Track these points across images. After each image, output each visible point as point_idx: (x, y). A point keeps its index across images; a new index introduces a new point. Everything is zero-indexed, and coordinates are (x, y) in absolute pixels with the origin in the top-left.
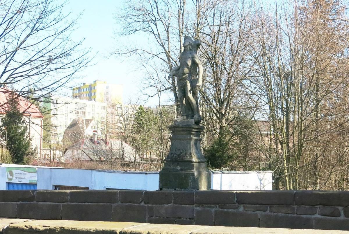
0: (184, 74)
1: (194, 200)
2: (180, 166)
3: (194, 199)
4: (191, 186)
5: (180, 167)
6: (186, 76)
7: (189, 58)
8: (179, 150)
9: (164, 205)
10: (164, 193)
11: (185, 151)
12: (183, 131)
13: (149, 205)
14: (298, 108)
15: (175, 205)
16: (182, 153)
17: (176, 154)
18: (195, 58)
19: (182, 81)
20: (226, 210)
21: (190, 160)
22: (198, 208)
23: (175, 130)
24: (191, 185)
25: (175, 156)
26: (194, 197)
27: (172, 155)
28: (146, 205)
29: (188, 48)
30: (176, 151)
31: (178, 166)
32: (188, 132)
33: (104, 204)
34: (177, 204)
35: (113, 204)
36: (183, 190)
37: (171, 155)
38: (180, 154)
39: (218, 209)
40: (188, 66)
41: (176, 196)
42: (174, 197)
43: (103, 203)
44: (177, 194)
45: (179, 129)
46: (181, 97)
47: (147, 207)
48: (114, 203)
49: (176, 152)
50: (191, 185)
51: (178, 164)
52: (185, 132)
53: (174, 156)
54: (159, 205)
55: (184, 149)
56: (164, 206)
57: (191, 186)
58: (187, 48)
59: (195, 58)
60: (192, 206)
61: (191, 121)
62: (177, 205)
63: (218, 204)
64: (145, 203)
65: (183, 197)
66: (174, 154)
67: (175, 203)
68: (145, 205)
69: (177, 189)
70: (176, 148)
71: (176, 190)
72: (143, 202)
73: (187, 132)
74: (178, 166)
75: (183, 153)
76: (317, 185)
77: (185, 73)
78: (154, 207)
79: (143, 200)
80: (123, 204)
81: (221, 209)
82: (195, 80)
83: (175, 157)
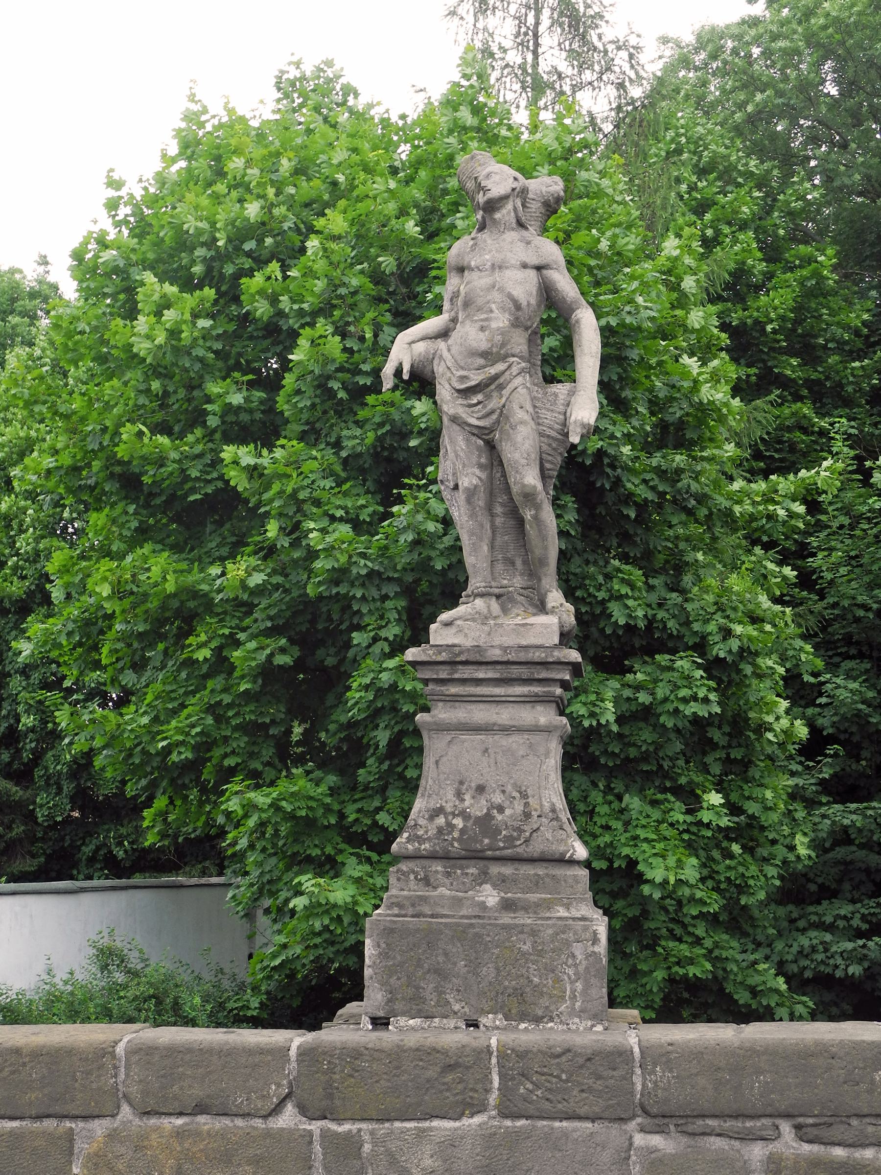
1: (632, 1093)
2: (495, 886)
3: (639, 1087)
4: (578, 1004)
5: (495, 893)
8: (481, 789)
9: (436, 1123)
10: (398, 1054)
11: (517, 795)
13: (333, 1126)
15: (508, 1123)
16: (501, 809)
17: (464, 814)
20: (839, 1152)
21: (562, 848)
22: (656, 1140)
24: (574, 998)
25: (459, 822)
26: (638, 1071)
27: (441, 821)
28: (315, 1127)
30: (459, 795)
31: (487, 887)
33: (15, 1124)
34: (519, 1117)
35: (81, 1124)
36: (523, 1026)
37: (431, 818)
38: (488, 816)
39: (789, 1143)
41: (517, 1063)
42: (501, 1076)
43: (12, 1118)
44: (522, 1054)
47: (316, 1137)
48: (85, 1118)
49: (463, 800)
50: (574, 998)
51: (484, 878)
53: (451, 826)
54: (397, 1124)
55: (509, 788)
56: (431, 1129)
57: (578, 1004)
60: (615, 1129)
62: (521, 1123)
63: (788, 1116)
64: (303, 1110)
65: (564, 1077)
66: (454, 815)
67: (504, 1114)
68: (309, 1128)
69: (484, 1020)
70: (461, 783)
71: (476, 1026)
72: (290, 1109)
74: (481, 884)
75: (508, 812)
76: (757, 792)
78: (366, 1137)
79: (288, 1096)
80: (153, 1121)
81: (806, 1148)
83: (463, 831)
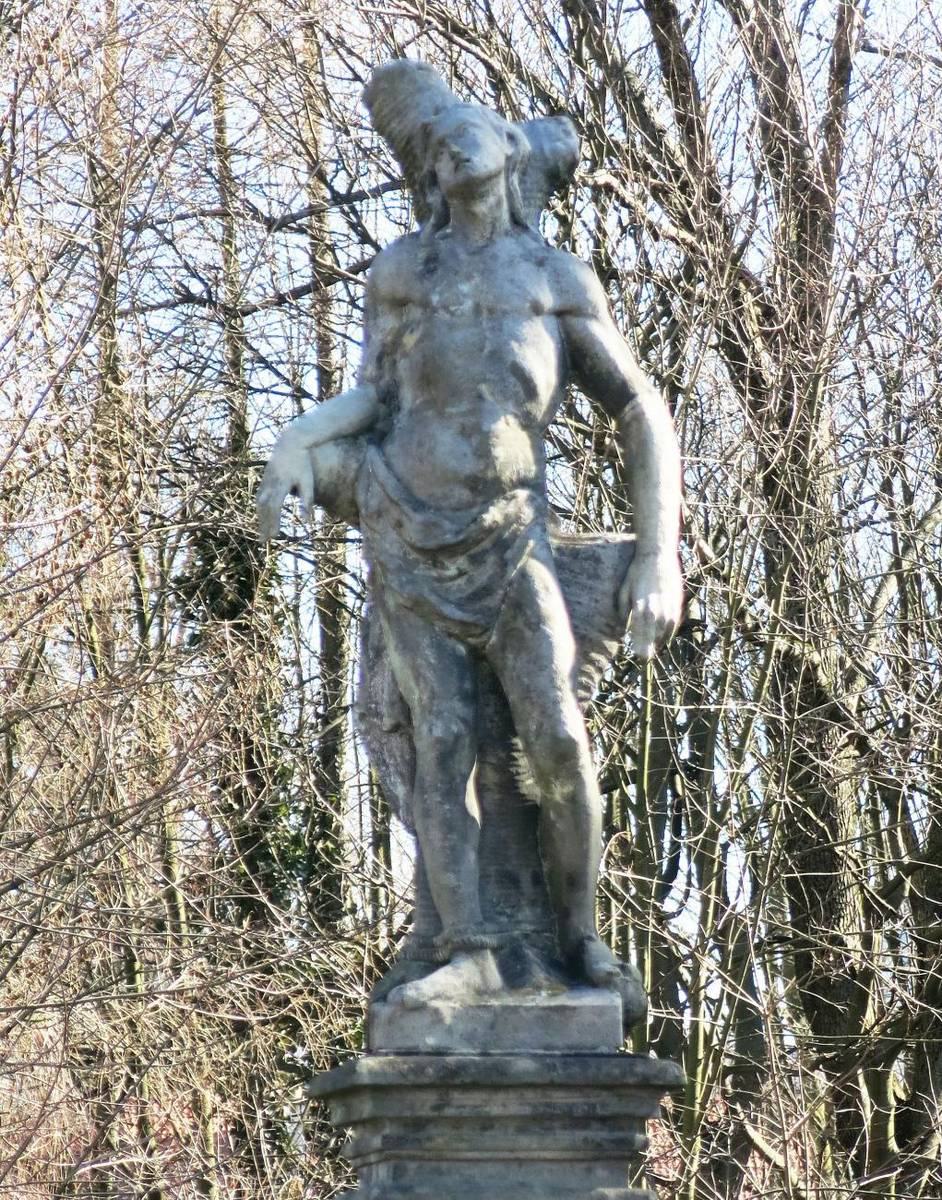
0: (488, 488)
6: (511, 509)
7: (537, 309)
12: (540, 1121)
14: (847, 295)
18: (594, 317)
19: (462, 562)
23: (449, 1112)
29: (499, 204)
32: (599, 1134)
40: (530, 406)
45: (499, 1105)
46: (458, 737)
52: (565, 1137)
58: (491, 200)
59: (594, 317)
61: (600, 1011)
73: (589, 1134)
77: (497, 480)
82: (597, 560)
